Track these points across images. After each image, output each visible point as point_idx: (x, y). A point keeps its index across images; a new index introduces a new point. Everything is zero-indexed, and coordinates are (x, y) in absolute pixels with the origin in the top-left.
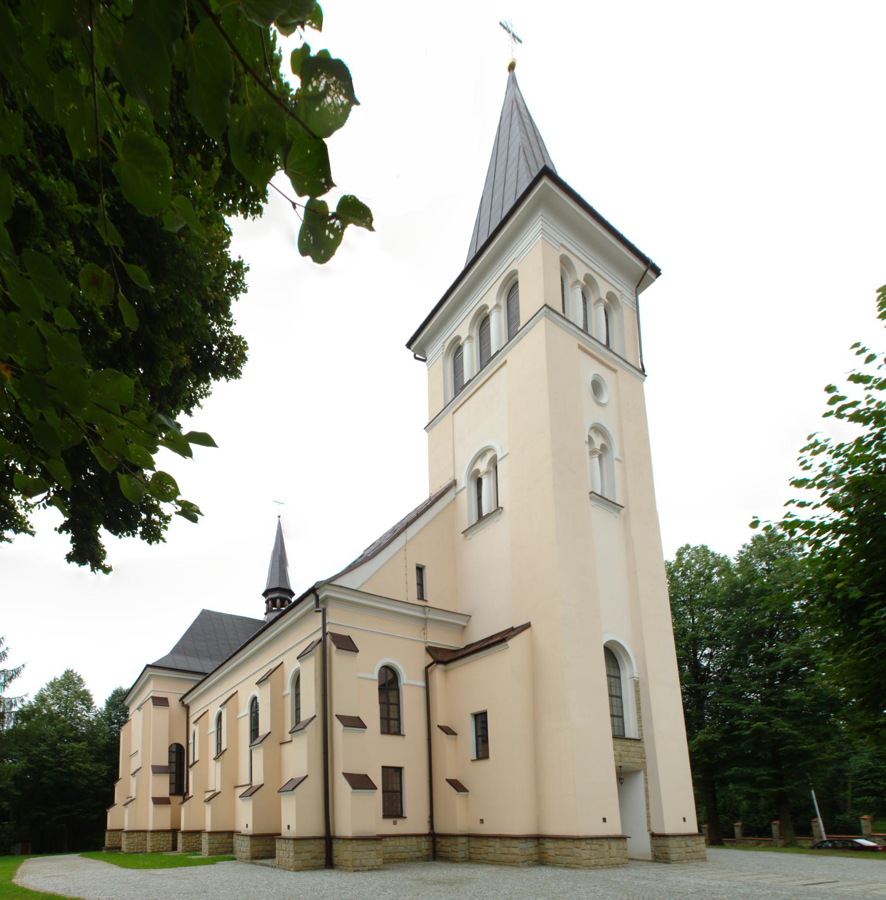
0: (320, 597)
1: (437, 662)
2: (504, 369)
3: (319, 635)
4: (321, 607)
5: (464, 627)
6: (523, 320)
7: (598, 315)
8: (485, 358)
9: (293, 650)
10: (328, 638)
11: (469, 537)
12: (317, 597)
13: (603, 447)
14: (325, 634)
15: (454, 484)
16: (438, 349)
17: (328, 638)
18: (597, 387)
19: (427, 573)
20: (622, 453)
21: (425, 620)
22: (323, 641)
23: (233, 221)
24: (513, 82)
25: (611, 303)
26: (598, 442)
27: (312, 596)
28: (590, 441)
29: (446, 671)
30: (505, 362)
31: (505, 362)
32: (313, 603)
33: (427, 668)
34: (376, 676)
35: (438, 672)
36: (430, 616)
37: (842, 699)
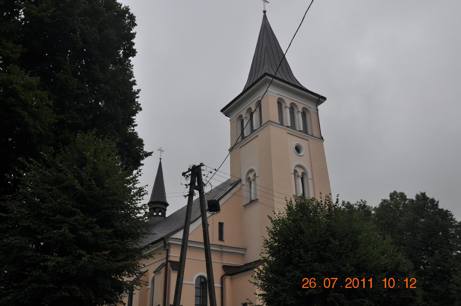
0: (167, 243)
1: (227, 274)
2: (257, 138)
3: (164, 261)
4: (167, 247)
5: (244, 254)
6: (192, 220)
7: (299, 118)
8: (252, 131)
9: (156, 264)
10: (169, 264)
11: (246, 209)
12: (165, 242)
13: (303, 174)
14: (167, 261)
15: (240, 181)
16: (235, 114)
17: (169, 264)
18: (298, 149)
19: (225, 227)
20: (313, 176)
21: (222, 251)
22: (165, 265)
23: (131, 58)
24: (265, 17)
25: (304, 113)
26: (300, 171)
27: (163, 241)
28: (295, 171)
29: (232, 279)
30: (258, 136)
31: (258, 136)
32: (163, 244)
33: (222, 277)
34: (194, 282)
35: (227, 280)
36: (224, 250)
37: (269, 264)
